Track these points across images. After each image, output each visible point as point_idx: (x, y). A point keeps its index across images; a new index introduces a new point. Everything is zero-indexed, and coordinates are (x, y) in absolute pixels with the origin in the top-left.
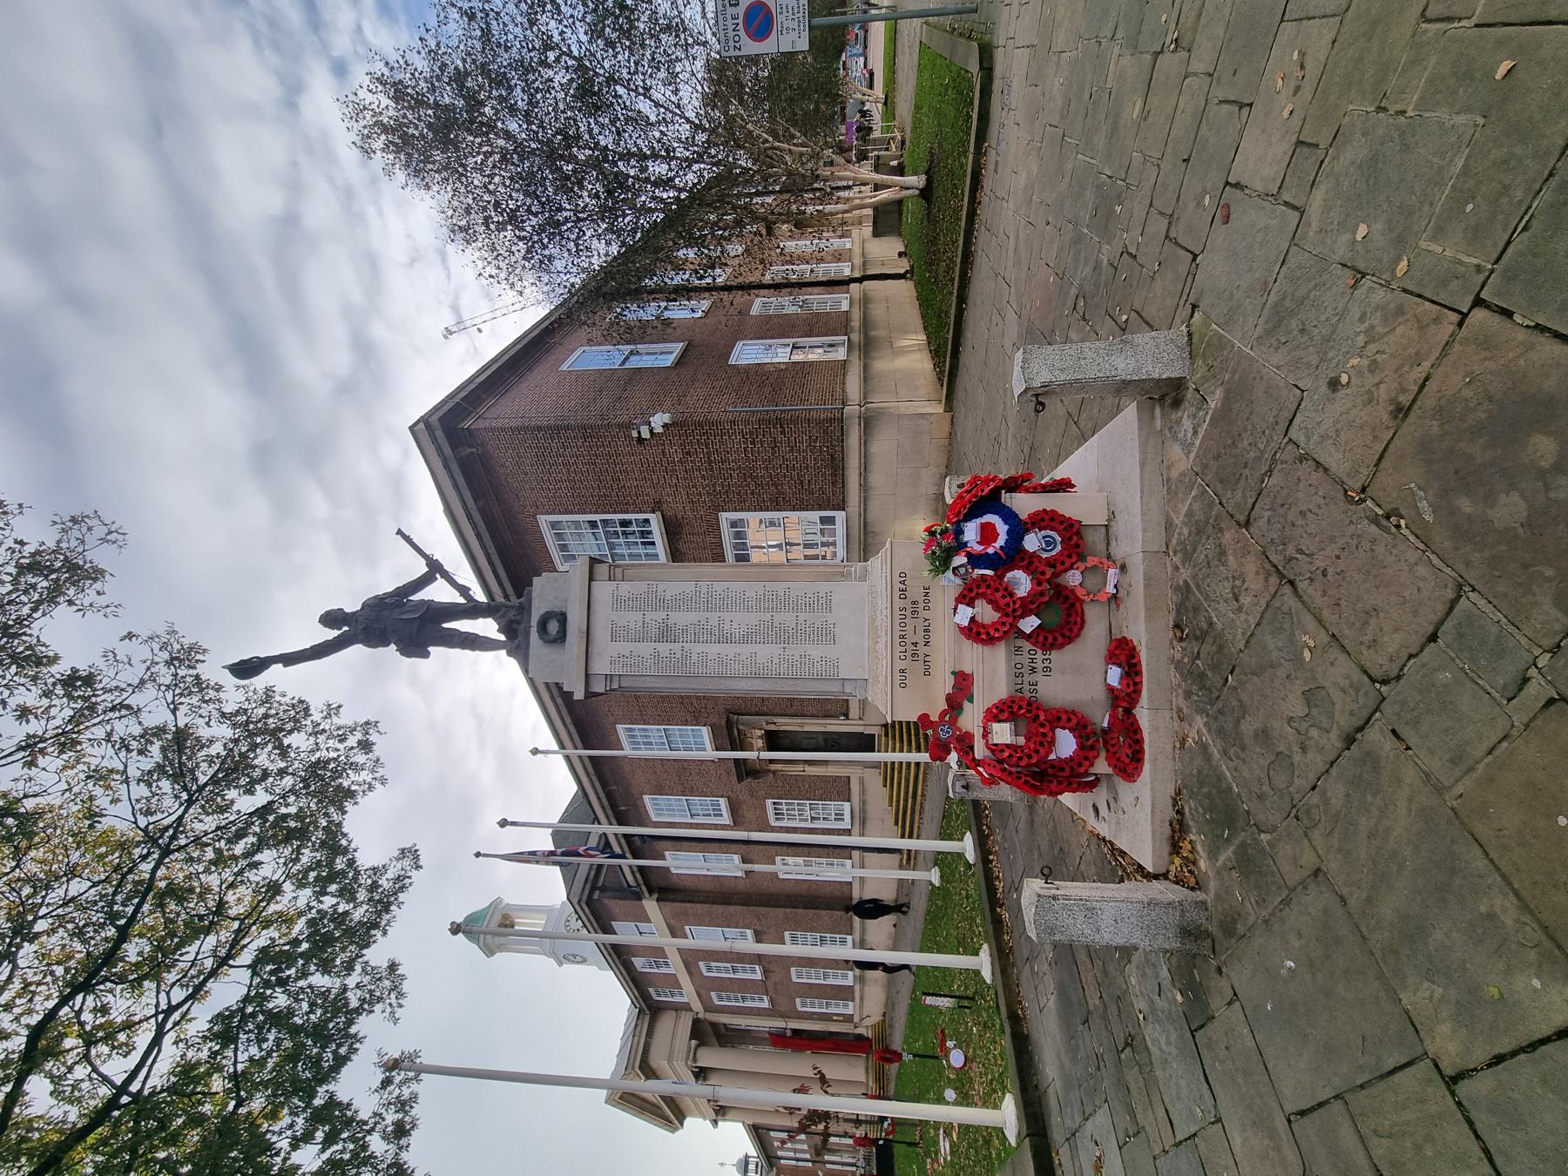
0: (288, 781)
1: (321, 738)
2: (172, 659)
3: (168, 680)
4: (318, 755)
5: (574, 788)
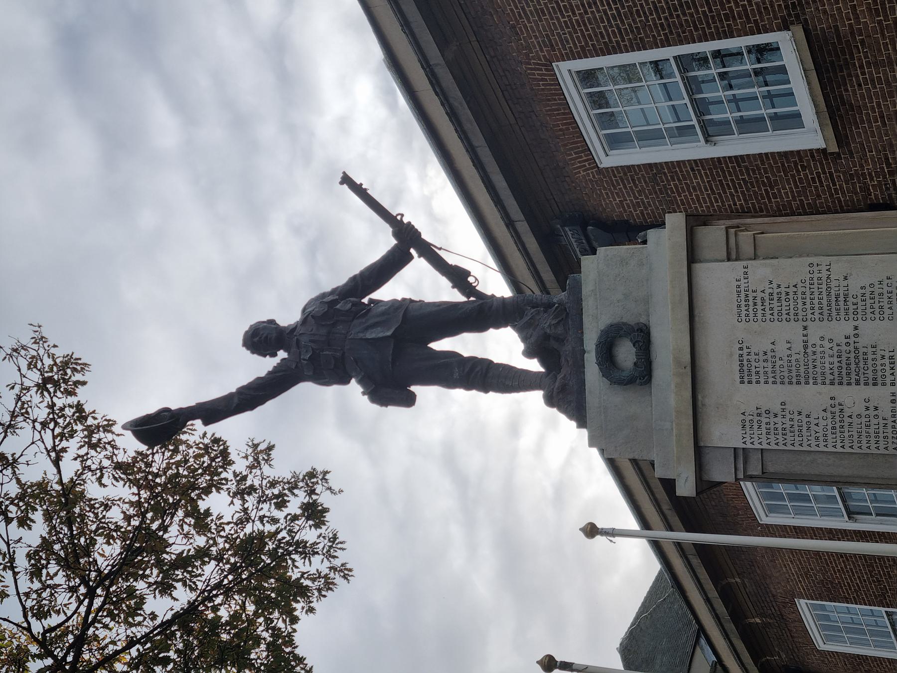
0: (210, 571)
1: (251, 500)
2: (46, 381)
3: (41, 413)
4: (248, 529)
5: (656, 566)
